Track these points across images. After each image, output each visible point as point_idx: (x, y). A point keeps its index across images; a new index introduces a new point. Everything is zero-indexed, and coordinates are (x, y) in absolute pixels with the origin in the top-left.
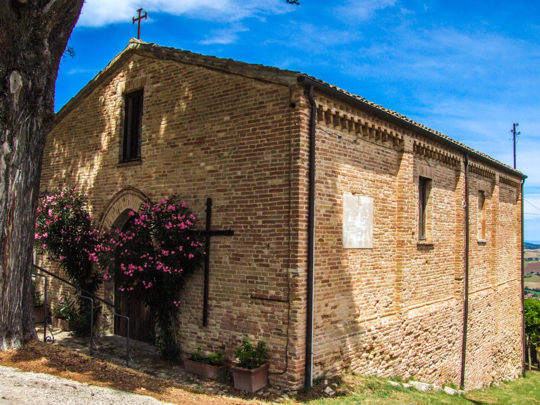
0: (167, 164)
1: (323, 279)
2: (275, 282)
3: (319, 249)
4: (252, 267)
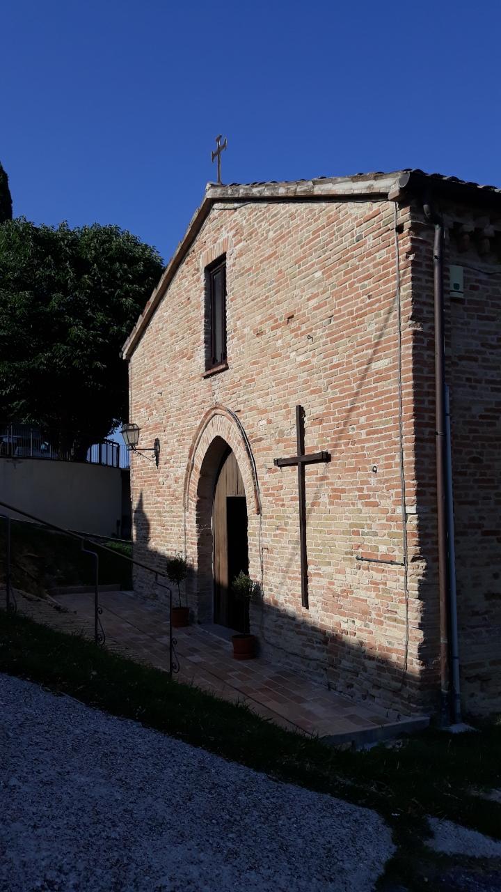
0: (254, 363)
1: (484, 529)
2: (386, 531)
3: (474, 474)
4: (356, 507)
